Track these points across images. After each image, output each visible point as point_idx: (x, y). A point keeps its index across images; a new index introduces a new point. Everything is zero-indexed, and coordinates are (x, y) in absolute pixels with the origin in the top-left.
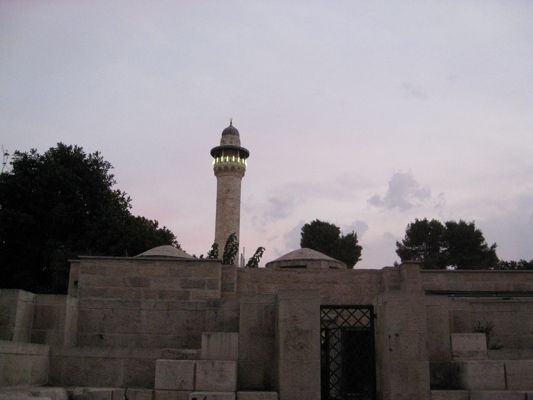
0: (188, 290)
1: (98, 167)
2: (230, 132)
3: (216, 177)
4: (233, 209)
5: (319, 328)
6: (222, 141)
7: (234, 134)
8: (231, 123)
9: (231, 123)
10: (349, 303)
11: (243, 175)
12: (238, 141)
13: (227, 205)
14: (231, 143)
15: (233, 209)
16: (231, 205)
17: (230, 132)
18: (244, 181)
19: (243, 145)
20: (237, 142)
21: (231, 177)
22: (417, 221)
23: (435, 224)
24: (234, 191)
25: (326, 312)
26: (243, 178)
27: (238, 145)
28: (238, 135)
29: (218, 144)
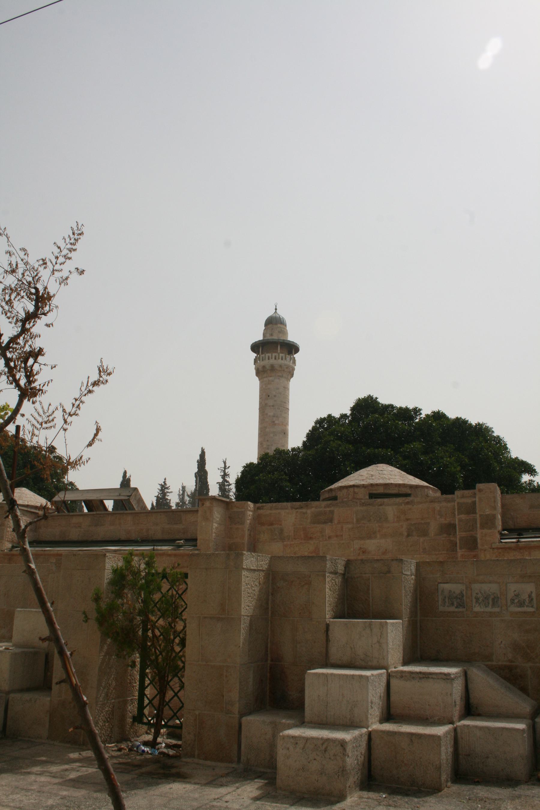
0: (332, 509)
1: (491, 442)
2: (274, 323)
3: (257, 378)
4: (274, 419)
5: (184, 730)
6: (264, 335)
7: (276, 324)
8: (276, 309)
9: (276, 309)
10: (468, 676)
11: (292, 375)
12: (285, 333)
13: (267, 414)
14: (272, 335)
15: (274, 419)
16: (271, 414)
17: (274, 323)
18: (293, 384)
19: (292, 337)
20: (279, 332)
21: (271, 378)
22: (376, 398)
23: (391, 406)
24: (275, 396)
25: (171, 713)
26: (292, 380)
27: (282, 338)
28: (286, 326)
29: (260, 338)
